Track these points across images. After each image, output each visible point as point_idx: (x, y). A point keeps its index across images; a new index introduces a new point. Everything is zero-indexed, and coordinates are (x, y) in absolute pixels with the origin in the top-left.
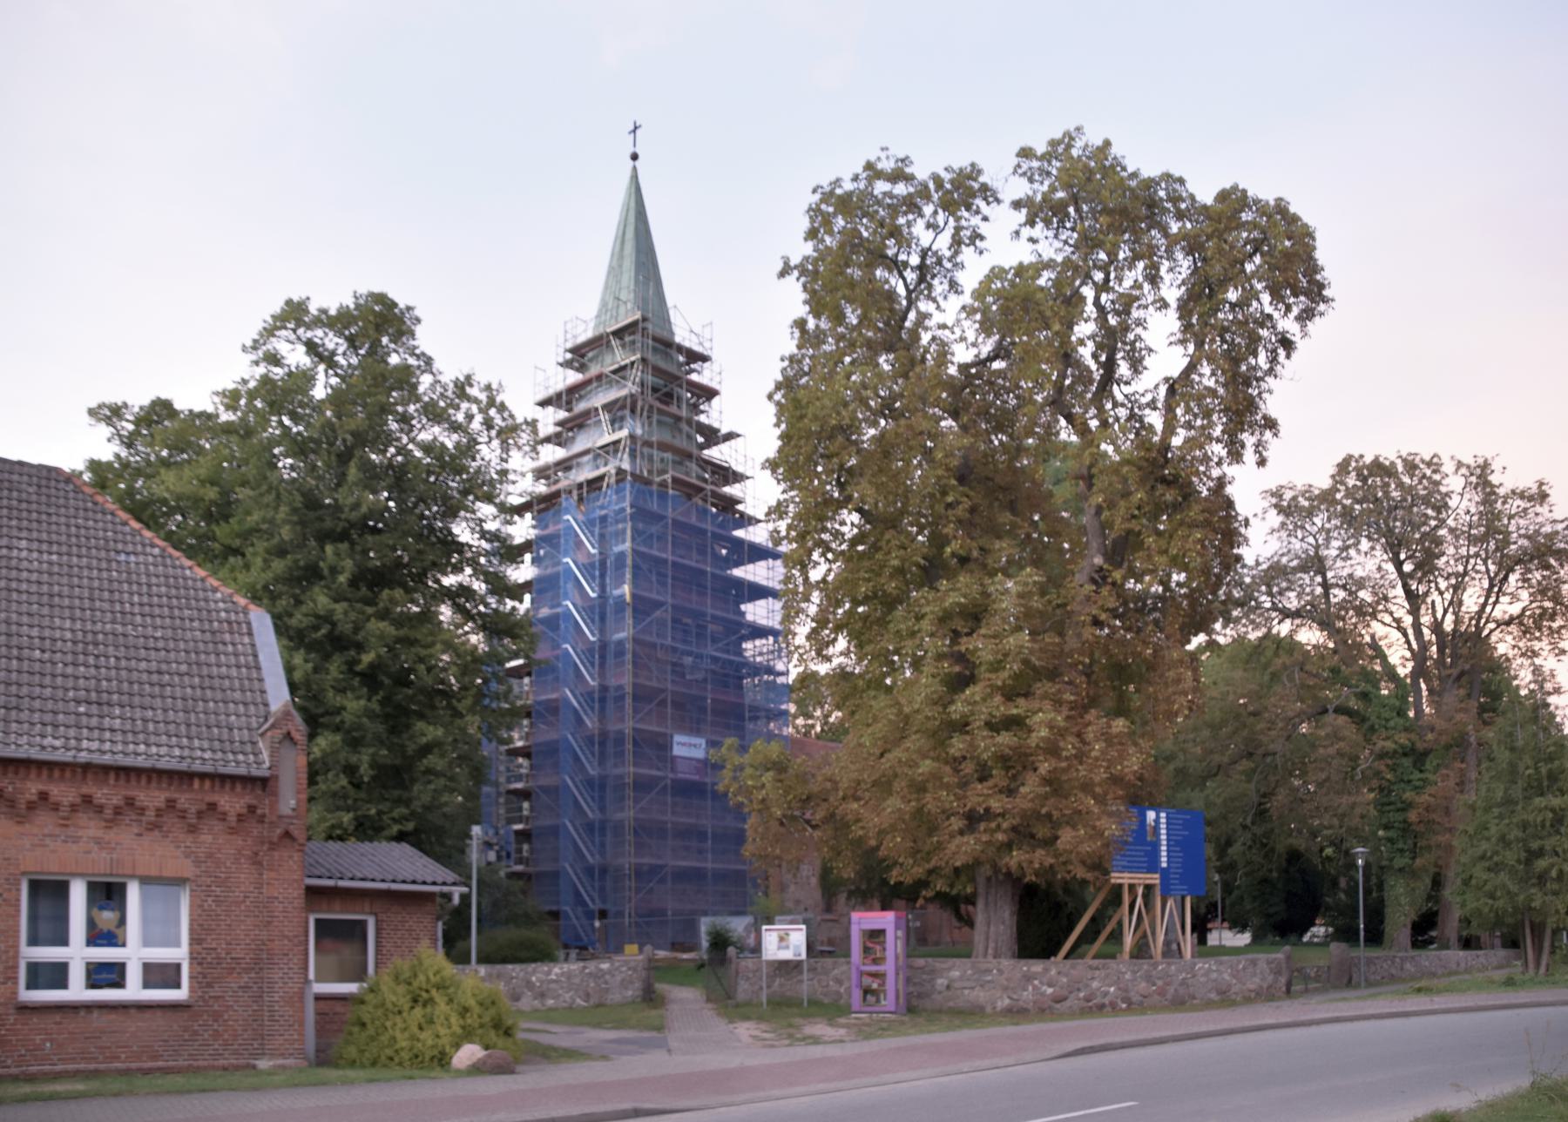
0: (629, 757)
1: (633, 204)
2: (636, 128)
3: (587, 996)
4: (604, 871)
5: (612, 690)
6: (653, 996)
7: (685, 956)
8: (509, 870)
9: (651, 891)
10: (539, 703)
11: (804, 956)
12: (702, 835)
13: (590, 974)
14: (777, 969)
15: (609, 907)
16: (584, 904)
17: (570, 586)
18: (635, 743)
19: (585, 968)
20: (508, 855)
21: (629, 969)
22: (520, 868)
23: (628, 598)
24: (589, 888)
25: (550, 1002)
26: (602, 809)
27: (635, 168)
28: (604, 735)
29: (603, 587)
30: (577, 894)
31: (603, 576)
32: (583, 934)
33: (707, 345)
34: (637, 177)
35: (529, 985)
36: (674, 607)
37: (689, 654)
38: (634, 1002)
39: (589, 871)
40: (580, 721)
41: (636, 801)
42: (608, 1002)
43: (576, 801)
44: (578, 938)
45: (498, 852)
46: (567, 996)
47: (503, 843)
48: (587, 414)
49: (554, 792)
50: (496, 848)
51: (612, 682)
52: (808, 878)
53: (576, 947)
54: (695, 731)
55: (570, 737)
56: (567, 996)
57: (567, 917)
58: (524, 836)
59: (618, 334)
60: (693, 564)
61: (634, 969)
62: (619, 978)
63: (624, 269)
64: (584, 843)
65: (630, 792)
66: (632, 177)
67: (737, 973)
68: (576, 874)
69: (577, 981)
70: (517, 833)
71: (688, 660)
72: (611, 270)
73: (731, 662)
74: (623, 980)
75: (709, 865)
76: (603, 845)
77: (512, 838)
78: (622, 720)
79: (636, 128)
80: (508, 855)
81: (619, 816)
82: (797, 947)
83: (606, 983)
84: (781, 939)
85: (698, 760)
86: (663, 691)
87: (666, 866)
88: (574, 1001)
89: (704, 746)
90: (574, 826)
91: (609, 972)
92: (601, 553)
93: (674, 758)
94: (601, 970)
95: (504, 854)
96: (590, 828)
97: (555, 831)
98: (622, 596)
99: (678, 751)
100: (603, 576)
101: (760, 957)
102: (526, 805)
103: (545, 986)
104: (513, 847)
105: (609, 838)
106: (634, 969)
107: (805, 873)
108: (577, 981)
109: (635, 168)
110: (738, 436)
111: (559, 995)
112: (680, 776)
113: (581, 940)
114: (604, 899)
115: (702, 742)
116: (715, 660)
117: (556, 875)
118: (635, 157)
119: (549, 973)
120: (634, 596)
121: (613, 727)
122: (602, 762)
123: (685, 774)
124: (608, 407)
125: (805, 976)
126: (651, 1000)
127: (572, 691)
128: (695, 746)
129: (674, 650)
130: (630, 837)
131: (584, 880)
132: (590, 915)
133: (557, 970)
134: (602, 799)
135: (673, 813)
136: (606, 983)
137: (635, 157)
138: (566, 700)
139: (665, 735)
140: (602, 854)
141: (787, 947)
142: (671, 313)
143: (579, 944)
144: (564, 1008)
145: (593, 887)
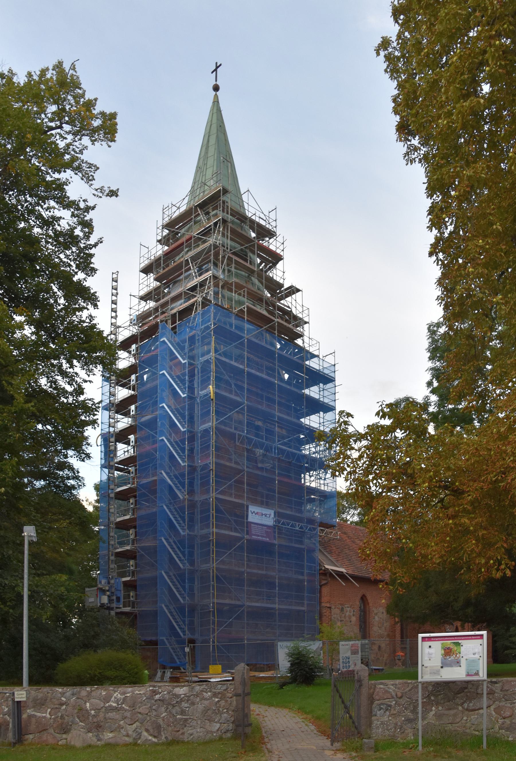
0: (213, 520)
1: (215, 120)
2: (217, 67)
3: (157, 730)
4: (192, 610)
5: (199, 469)
6: (248, 730)
7: (262, 675)
8: (119, 610)
9: (230, 625)
10: (142, 486)
11: (483, 675)
12: (271, 585)
13: (161, 700)
14: (431, 693)
15: (196, 636)
16: (177, 635)
17: (166, 394)
18: (218, 511)
19: (155, 692)
20: (118, 599)
21: (215, 695)
22: (128, 609)
23: (212, 396)
24: (181, 623)
25: (108, 736)
26: (192, 563)
27: (216, 96)
28: (192, 505)
29: (191, 389)
30: (172, 628)
31: (191, 381)
32: (176, 658)
33: (274, 224)
34: (219, 111)
35: (82, 713)
36: (250, 409)
37: (261, 446)
38: (221, 739)
39: (181, 610)
40: (174, 496)
41: (218, 555)
42: (186, 738)
43: (171, 559)
44: (173, 661)
45: (109, 596)
46: (130, 729)
47: (113, 590)
48: (179, 267)
49: (153, 552)
50: (108, 593)
51: (199, 463)
52: (350, 617)
53: (171, 668)
54: (265, 503)
55: (165, 507)
56: (130, 729)
57: (164, 644)
58: (130, 586)
59: (203, 206)
60: (264, 376)
61: (222, 696)
62: (200, 707)
63: (210, 154)
64: (177, 589)
65: (213, 548)
66: (214, 102)
67: (371, 700)
68: (171, 613)
69: (143, 709)
70: (125, 583)
71: (259, 452)
72: (199, 169)
73: (294, 454)
74: (206, 710)
75: (277, 606)
76: (191, 589)
77: (122, 587)
78: (208, 491)
79: (217, 67)
80: (118, 599)
81: (204, 567)
82: (471, 662)
83: (183, 712)
84: (448, 652)
85: (268, 527)
86: (240, 471)
87: (243, 605)
88: (140, 734)
89: (272, 516)
90: (169, 576)
91: (188, 698)
92: (190, 364)
93: (249, 524)
94: (177, 696)
95: (114, 598)
96: (181, 577)
97: (154, 581)
98: (208, 394)
99: (252, 518)
100: (191, 381)
101: (415, 676)
102: (132, 562)
103: (102, 715)
104: (122, 594)
105: (197, 585)
106: (222, 696)
107: (347, 614)
108: (143, 709)
109: (216, 96)
110: (298, 290)
111: (121, 727)
112: (254, 537)
113: (174, 662)
114: (192, 630)
115: (272, 512)
116: (281, 451)
117: (155, 614)
118: (216, 88)
119: (107, 699)
120: (216, 394)
121: (199, 498)
122: (191, 527)
123: (257, 535)
124: (194, 259)
125: (485, 701)
126: (246, 736)
127: (167, 473)
128: (266, 515)
129: (250, 441)
130: (213, 583)
131: (177, 617)
132: (181, 642)
133: (117, 695)
134: (191, 554)
135: (248, 566)
136: (183, 712)
137: (216, 88)
138: (163, 481)
139: (243, 505)
140: (192, 595)
141: (458, 663)
142: (245, 197)
143: (173, 665)
144: (126, 745)
145: (184, 622)
